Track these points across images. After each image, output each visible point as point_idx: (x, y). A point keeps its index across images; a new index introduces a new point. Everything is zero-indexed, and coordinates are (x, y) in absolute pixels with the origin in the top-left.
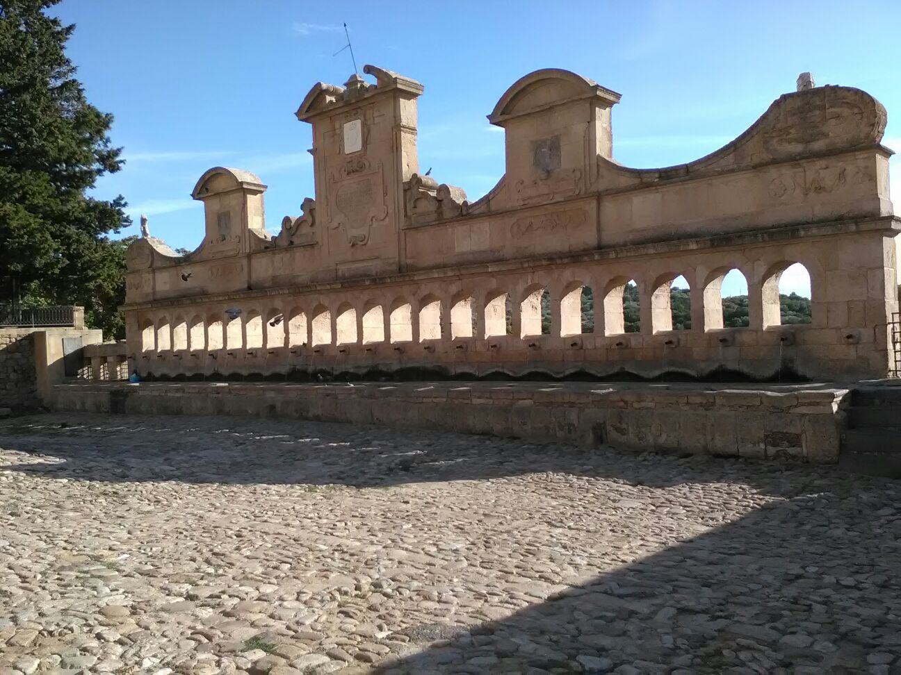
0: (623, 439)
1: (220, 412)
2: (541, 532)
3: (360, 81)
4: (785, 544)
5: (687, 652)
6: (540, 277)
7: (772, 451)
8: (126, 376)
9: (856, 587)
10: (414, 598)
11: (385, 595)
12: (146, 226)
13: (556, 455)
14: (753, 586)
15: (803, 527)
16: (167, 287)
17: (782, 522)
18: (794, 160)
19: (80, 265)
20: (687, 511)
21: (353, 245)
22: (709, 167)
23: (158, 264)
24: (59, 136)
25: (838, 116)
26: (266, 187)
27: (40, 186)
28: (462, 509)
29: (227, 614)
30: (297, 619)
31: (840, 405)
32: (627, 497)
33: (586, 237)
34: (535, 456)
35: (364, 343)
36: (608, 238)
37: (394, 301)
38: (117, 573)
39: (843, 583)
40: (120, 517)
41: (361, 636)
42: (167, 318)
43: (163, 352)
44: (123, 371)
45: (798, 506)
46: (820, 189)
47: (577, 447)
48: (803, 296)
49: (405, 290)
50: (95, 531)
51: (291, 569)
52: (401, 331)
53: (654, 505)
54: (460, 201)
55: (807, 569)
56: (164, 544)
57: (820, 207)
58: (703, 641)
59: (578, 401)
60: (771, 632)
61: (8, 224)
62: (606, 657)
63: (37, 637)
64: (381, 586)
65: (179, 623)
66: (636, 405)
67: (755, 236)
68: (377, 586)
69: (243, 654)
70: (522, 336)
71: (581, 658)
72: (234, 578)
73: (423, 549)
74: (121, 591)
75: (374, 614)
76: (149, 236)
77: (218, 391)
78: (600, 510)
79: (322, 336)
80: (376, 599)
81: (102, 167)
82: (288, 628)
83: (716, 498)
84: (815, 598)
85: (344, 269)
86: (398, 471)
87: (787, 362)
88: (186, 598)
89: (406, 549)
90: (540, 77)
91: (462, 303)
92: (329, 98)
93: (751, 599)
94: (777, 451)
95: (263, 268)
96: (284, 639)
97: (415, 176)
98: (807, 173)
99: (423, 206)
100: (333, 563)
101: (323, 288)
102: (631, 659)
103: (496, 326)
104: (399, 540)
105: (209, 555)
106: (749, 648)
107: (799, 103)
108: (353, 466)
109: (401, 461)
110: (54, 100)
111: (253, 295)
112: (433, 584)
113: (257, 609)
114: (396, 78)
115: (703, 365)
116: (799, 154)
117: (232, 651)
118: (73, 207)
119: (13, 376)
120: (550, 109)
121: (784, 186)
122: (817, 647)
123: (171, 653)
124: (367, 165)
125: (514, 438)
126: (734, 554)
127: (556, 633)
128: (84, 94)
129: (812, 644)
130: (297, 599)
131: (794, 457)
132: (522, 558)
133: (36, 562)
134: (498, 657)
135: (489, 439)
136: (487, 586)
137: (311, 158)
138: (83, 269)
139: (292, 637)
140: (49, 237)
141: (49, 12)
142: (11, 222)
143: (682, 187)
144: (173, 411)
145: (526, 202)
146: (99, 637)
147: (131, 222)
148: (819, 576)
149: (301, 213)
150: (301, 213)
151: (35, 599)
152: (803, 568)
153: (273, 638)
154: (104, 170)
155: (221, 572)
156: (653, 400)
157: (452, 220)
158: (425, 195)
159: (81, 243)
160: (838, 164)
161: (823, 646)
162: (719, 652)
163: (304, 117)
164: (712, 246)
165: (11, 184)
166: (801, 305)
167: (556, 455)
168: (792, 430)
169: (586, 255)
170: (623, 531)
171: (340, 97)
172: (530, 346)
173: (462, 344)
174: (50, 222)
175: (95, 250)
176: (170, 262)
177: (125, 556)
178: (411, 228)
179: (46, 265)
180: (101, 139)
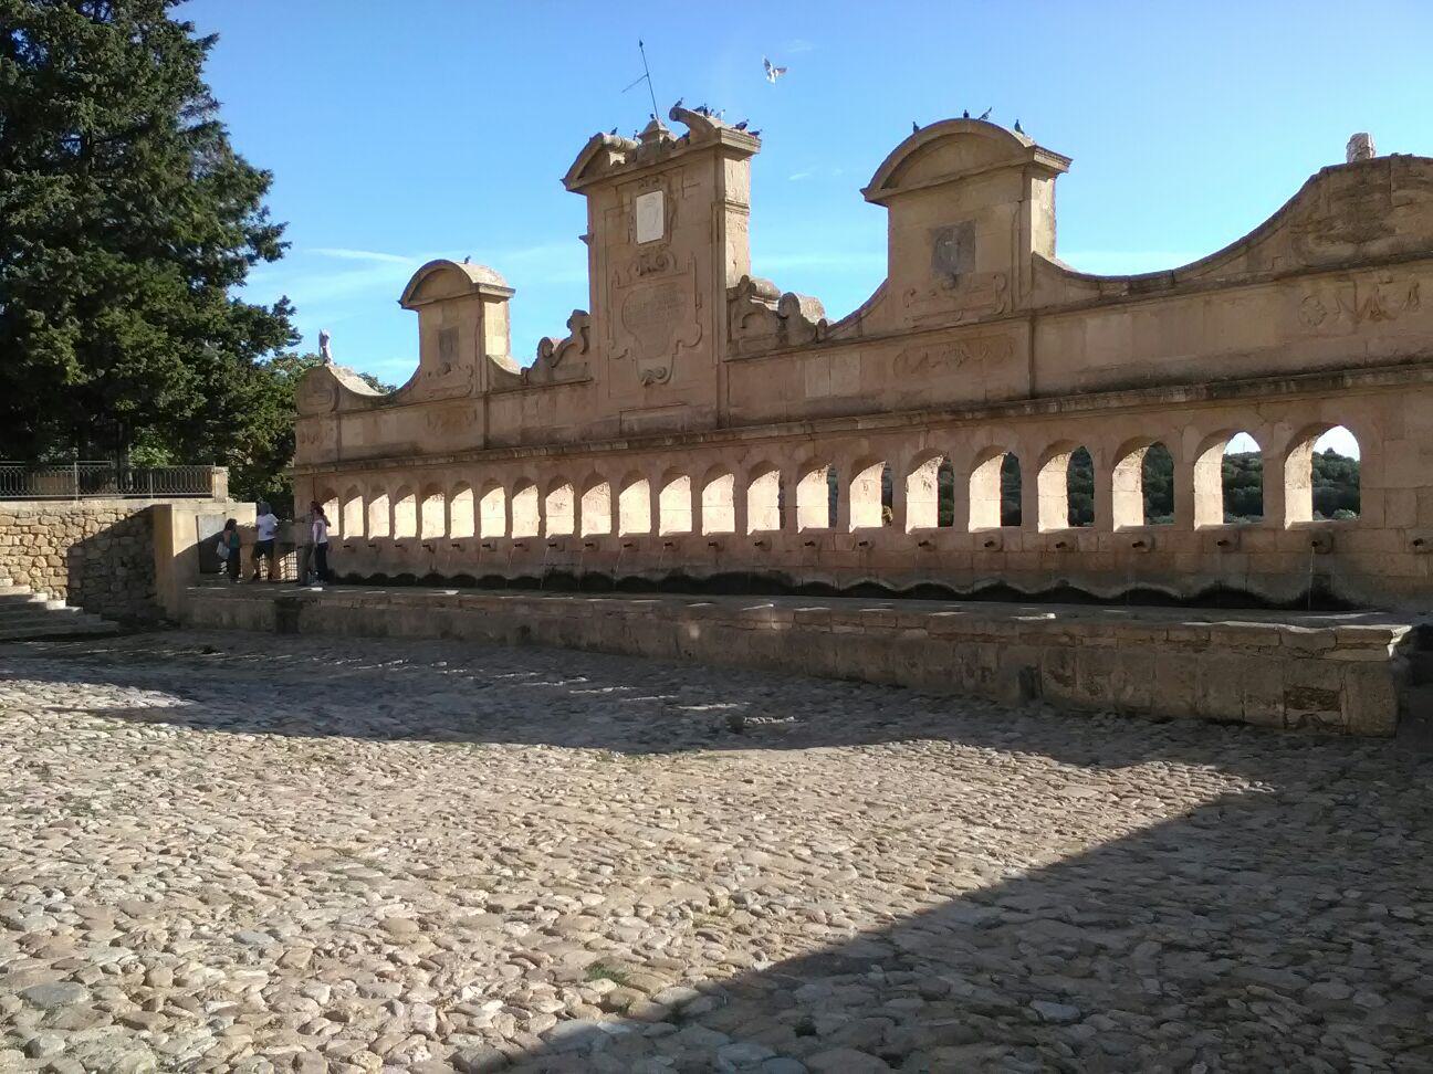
0: (1067, 692)
1: (445, 634)
2: (955, 831)
3: (663, 132)
4: (1313, 857)
5: (1181, 1002)
6: (940, 438)
7: (1294, 715)
8: (294, 575)
9: (1416, 921)
10: (795, 918)
11: (753, 913)
12: (328, 346)
13: (963, 715)
14: (1268, 916)
15: (1340, 833)
16: (360, 442)
17: (1308, 824)
18: (1339, 269)
19: (223, 404)
20: (1169, 805)
21: (647, 384)
22: (1207, 276)
23: (345, 405)
24: (195, 208)
25: (1410, 203)
26: (513, 291)
27: (165, 283)
28: (832, 794)
29: (549, 933)
30: (644, 941)
31: (1397, 646)
32: (1076, 781)
33: (1012, 378)
34: (931, 715)
35: (661, 533)
36: (1047, 382)
37: (710, 469)
38: (381, 874)
39: (1396, 914)
40: (352, 794)
41: (735, 966)
42: (359, 487)
43: (353, 540)
44: (289, 567)
45: (1333, 800)
46: (1377, 315)
47: (995, 703)
48: (1346, 455)
49: (728, 453)
50: (325, 814)
51: (615, 873)
52: (719, 517)
53: (1117, 795)
54: (814, 319)
55: (1346, 893)
56: (430, 833)
57: (1378, 342)
58: (1198, 987)
59: (998, 634)
60: (1294, 977)
61: (118, 340)
62: (1070, 1004)
63: (312, 958)
64: (744, 902)
65: (488, 942)
66: (1087, 641)
67: (1276, 383)
68: (738, 900)
69: (588, 984)
70: (908, 529)
71: (1037, 1005)
72: (542, 884)
73: (791, 852)
74: (398, 898)
75: (745, 939)
76: (332, 363)
77: (442, 602)
78: (1037, 800)
79: (596, 522)
80: (742, 918)
81: (254, 253)
82: (635, 952)
83: (1209, 786)
84: (1355, 934)
85: (632, 421)
86: (726, 733)
87: (1321, 577)
88: (487, 910)
89: (768, 851)
90: (947, 131)
91: (814, 475)
92: (614, 157)
93: (1265, 934)
94: (1303, 716)
95: (507, 417)
96: (635, 967)
97: (745, 279)
98: (1359, 289)
99: (758, 326)
100: (671, 867)
101: (599, 448)
102: (1103, 1007)
103: (866, 512)
104: (753, 837)
105: (496, 851)
106: (1263, 998)
107: (1349, 180)
108: (659, 723)
109: (729, 719)
110: (184, 149)
111: (491, 457)
112: (816, 900)
113: (587, 926)
114: (720, 129)
115: (1190, 580)
116: (1347, 260)
117: (573, 981)
118: (215, 316)
119: (121, 571)
120: (958, 181)
121: (1323, 307)
122: (1358, 999)
123: (494, 981)
124: (672, 262)
125: (896, 687)
126: (1238, 870)
127: (997, 972)
128: (228, 139)
129: (1352, 994)
130: (636, 915)
131: (1327, 725)
132: (934, 868)
133: (266, 857)
134: (925, 1000)
135: (859, 688)
136: (892, 905)
137: (585, 247)
138: (228, 411)
139: (645, 965)
140: (179, 362)
141: (174, 14)
142: (123, 338)
143: (1163, 305)
144: (370, 634)
145: (917, 324)
146: (392, 958)
147: (301, 337)
148: (1363, 904)
149: (567, 333)
150: (567, 333)
151: (288, 908)
152: (1340, 891)
153: (620, 965)
154: (257, 257)
155: (521, 874)
156: (1115, 634)
157: (804, 348)
158: (761, 310)
159: (226, 371)
160: (1404, 277)
161: (1367, 998)
162: (1223, 1003)
163: (576, 185)
164: (1210, 398)
165: (123, 279)
166: (1342, 469)
167: (963, 715)
168: (1326, 685)
169: (1012, 408)
170: (1074, 833)
171: (632, 155)
172: (920, 545)
173: (813, 539)
174: (180, 339)
175: (245, 381)
176: (364, 403)
177: (384, 850)
178: (736, 360)
179: (171, 404)
180: (254, 209)
